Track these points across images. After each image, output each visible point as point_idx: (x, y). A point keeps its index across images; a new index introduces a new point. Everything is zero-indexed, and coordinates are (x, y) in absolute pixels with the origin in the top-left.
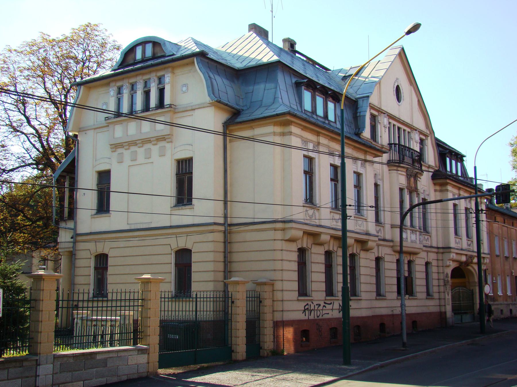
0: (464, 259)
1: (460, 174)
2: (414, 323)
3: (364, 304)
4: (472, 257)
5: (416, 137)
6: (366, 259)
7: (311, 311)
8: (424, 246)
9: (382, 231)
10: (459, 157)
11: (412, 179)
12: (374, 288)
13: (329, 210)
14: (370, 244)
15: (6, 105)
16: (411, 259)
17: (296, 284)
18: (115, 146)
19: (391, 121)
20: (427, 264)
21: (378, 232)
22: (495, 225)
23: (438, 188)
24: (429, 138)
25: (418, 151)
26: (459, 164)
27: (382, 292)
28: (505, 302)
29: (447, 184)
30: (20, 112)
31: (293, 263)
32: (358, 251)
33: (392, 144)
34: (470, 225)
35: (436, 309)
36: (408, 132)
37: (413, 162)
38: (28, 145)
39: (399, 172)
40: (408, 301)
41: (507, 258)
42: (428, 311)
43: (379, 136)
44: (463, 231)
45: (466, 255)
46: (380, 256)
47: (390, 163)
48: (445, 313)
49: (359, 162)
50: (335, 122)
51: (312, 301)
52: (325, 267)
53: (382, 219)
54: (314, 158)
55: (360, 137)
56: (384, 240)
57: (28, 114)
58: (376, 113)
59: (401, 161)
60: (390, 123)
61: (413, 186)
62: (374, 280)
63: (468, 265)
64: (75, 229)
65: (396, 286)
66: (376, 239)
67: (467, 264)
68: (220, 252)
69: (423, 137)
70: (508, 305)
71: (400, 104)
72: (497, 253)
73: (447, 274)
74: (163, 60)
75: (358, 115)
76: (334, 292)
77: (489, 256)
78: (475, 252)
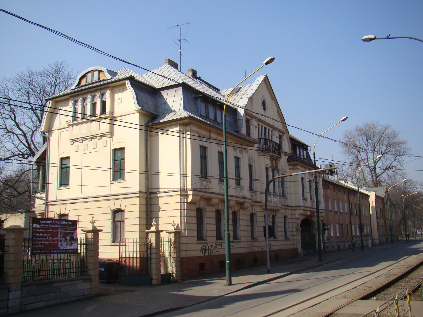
0: (309, 213)
1: (305, 157)
2: (277, 256)
3: (242, 245)
4: (314, 212)
5: (276, 133)
6: (244, 214)
7: (206, 250)
8: (283, 205)
10: (305, 147)
11: (274, 161)
14: (246, 205)
15: (4, 115)
17: (196, 232)
18: (74, 141)
19: (259, 123)
20: (285, 217)
21: (252, 197)
22: (329, 192)
23: (291, 167)
24: (285, 135)
25: (278, 143)
26: (305, 152)
27: (255, 236)
28: (335, 241)
29: (296, 165)
30: (12, 119)
31: (193, 218)
32: (238, 209)
33: (260, 138)
34: (312, 191)
35: (291, 247)
36: (271, 131)
37: (275, 150)
38: (17, 142)
39: (266, 157)
41: (336, 212)
42: (286, 248)
44: (308, 196)
45: (310, 211)
46: (253, 212)
47: (259, 150)
48: (297, 249)
49: (238, 150)
53: (254, 187)
55: (220, 93)
56: (256, 202)
57: (17, 121)
58: (249, 118)
60: (259, 125)
62: (249, 228)
63: (311, 218)
65: (263, 232)
66: (250, 201)
67: (311, 216)
69: (282, 134)
70: (337, 242)
72: (330, 209)
73: (298, 223)
74: (105, 82)
75: (238, 119)
76: (222, 237)
77: (325, 211)
78: (315, 208)
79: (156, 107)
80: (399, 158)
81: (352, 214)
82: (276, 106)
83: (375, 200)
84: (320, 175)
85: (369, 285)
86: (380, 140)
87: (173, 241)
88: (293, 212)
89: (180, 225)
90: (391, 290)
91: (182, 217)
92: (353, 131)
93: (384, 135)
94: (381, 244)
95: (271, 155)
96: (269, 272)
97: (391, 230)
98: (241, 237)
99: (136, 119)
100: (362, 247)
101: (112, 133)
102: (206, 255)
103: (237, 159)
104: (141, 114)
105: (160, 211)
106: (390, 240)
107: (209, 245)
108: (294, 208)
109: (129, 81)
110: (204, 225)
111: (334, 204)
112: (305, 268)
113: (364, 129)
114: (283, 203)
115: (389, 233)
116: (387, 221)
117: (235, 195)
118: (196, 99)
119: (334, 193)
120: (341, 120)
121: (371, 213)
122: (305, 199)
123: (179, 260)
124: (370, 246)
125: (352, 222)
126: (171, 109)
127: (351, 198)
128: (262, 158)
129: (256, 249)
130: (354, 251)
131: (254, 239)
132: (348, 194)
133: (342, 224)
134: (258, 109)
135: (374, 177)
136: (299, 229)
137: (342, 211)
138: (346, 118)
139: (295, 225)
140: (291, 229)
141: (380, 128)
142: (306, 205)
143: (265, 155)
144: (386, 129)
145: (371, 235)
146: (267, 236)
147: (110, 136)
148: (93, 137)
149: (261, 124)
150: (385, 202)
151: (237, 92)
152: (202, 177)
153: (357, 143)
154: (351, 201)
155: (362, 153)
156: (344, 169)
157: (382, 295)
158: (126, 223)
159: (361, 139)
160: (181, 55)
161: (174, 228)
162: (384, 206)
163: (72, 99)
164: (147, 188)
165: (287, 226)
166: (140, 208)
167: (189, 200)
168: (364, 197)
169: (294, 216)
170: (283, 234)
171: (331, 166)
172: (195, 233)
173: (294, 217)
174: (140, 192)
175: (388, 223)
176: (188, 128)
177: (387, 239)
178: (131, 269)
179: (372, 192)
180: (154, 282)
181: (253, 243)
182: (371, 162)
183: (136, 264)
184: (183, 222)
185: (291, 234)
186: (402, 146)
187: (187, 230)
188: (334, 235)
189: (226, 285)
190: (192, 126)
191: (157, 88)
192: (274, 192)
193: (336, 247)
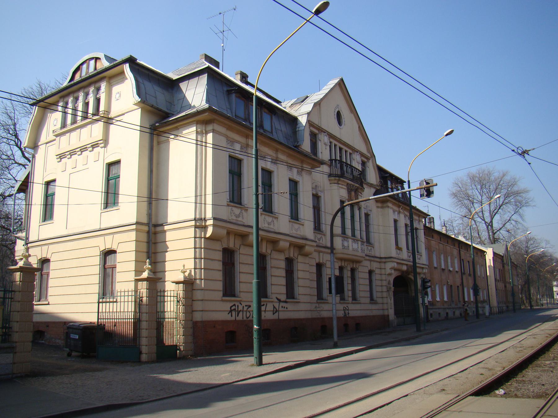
0: (404, 268)
3: (302, 307)
7: (239, 312)
8: (366, 255)
9: (324, 239)
14: (307, 249)
16: (355, 266)
18: (61, 157)
19: (331, 140)
20: (370, 272)
22: (433, 243)
23: (379, 205)
24: (371, 161)
28: (442, 307)
32: (296, 255)
36: (350, 154)
39: (340, 186)
40: (352, 305)
41: (443, 270)
42: (371, 314)
43: (320, 152)
45: (407, 265)
46: (321, 261)
48: (388, 316)
49: (295, 170)
50: (272, 132)
51: (240, 302)
58: (316, 131)
59: (342, 175)
60: (331, 142)
64: (27, 238)
67: (407, 272)
68: (144, 252)
75: (297, 129)
79: (171, 104)
80: (520, 211)
81: (464, 274)
83: (493, 258)
84: (421, 219)
85: (489, 366)
86: (497, 188)
87: (181, 295)
88: (383, 265)
89: (193, 271)
90: (530, 373)
92: (465, 178)
93: (502, 182)
94: (501, 312)
95: (348, 184)
96: (335, 346)
97: (513, 295)
98: (300, 296)
99: (136, 117)
100: (477, 315)
101: (106, 141)
102: (238, 319)
103: (294, 184)
104: (144, 111)
105: (167, 251)
106: (511, 308)
108: (383, 260)
109: (128, 65)
110: (237, 275)
111: (440, 259)
112: (392, 340)
113: (478, 175)
114: (367, 252)
115: (510, 299)
116: (507, 285)
117: (288, 233)
118: (229, 92)
119: (441, 245)
120: (445, 134)
121: (488, 274)
122: (398, 248)
124: (487, 314)
125: (465, 284)
126: (190, 105)
127: (462, 253)
128: (335, 186)
129: (325, 314)
130: (466, 320)
131: (322, 299)
132: (459, 247)
133: (451, 286)
135: (491, 234)
136: (390, 288)
137: (451, 269)
138: (452, 132)
139: (385, 283)
140: (379, 289)
141: (496, 174)
142: (401, 257)
144: (504, 175)
145: (488, 301)
146: (333, 291)
147: (103, 145)
148: (83, 149)
149: (334, 142)
150: (505, 261)
151: (302, 102)
152: (232, 201)
153: (470, 192)
154: (463, 257)
155: (476, 205)
156: (454, 225)
157: (515, 384)
158: (118, 269)
159: (473, 186)
160: (224, 50)
161: (185, 277)
162: (503, 267)
163: (62, 100)
164: (150, 215)
165: (374, 284)
166: (137, 246)
167: (209, 234)
168: (479, 253)
170: (368, 294)
171: (427, 183)
172: (219, 286)
174: (137, 223)
175: (509, 287)
176: (210, 127)
177: (507, 307)
178: (122, 337)
179: (489, 249)
180: (144, 357)
181: (321, 305)
182: (487, 215)
183: (129, 331)
184: (198, 267)
185: (379, 295)
186: (524, 195)
187: (204, 279)
189: (253, 365)
190: (215, 125)
191: (174, 79)
192: (353, 235)
193: (443, 315)
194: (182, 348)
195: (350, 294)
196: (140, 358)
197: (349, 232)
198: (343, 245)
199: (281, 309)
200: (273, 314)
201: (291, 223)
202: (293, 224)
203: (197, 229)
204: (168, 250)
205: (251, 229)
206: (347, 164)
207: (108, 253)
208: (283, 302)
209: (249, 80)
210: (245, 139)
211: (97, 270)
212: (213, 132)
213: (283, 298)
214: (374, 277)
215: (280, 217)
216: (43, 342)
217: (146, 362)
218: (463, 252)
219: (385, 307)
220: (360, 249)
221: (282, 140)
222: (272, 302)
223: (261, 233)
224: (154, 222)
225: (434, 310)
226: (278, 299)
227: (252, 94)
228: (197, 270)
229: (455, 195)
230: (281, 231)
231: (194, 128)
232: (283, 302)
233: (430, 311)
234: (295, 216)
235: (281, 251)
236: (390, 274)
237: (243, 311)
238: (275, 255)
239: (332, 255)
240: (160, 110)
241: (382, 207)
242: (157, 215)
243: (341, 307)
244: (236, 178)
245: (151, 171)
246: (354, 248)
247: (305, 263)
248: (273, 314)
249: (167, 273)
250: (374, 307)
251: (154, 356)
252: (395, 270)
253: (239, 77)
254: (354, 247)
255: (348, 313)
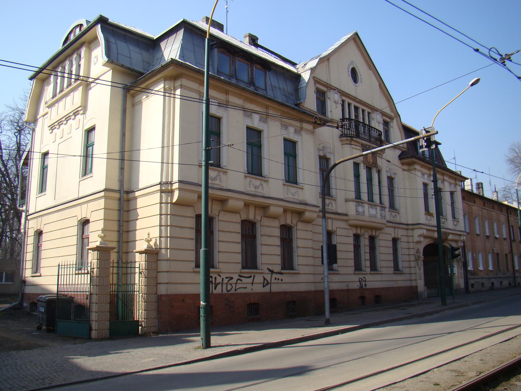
3: (302, 278)
8: (388, 222)
9: (398, 217)
12: (391, 264)
13: (281, 183)
14: (308, 215)
16: (374, 234)
18: (52, 128)
19: (344, 98)
20: (395, 241)
23: (406, 167)
24: (395, 121)
28: (487, 276)
32: (295, 222)
36: (369, 113)
39: (353, 146)
41: (488, 237)
42: (395, 285)
46: (397, 237)
48: (416, 287)
49: (256, 117)
50: (266, 90)
52: (281, 241)
54: (263, 131)
58: (324, 89)
59: (358, 136)
61: (371, 161)
71: (356, 85)
73: (418, 250)
75: (299, 87)
81: (514, 241)
82: (377, 79)
88: (410, 233)
89: (158, 239)
91: (163, 228)
96: (328, 323)
101: (84, 107)
104: (115, 72)
107: (223, 276)
108: (411, 227)
111: (493, 226)
114: (388, 218)
119: (484, 210)
123: (154, 298)
132: (507, 213)
134: (341, 80)
137: (497, 236)
139: (412, 252)
140: (406, 258)
142: (458, 228)
143: (352, 143)
147: (81, 112)
148: (67, 118)
149: (347, 100)
154: (512, 223)
160: (227, 12)
164: (121, 182)
169: (411, 239)
171: (427, 132)
173: (411, 239)
174: (105, 190)
176: (178, 83)
180: (94, 334)
184: (163, 235)
185: (406, 264)
188: (483, 267)
189: (199, 348)
190: (183, 79)
193: (487, 284)
194: (143, 323)
195: (368, 263)
196: (90, 334)
197: (365, 197)
198: (357, 211)
199: (273, 281)
200: (264, 287)
201: (286, 187)
202: (289, 188)
203: (163, 194)
204: (139, 218)
205: (199, 187)
206: (364, 124)
207: (85, 223)
208: (277, 273)
209: (259, 42)
210: (225, 95)
211: (74, 240)
212: (181, 88)
213: (278, 268)
214: (400, 245)
215: (306, 187)
216: (36, 313)
217: (95, 339)
218: (512, 219)
219: (413, 277)
220: (379, 216)
221: (280, 98)
222: (263, 273)
223: (210, 191)
224: (126, 188)
225: (476, 280)
226: (269, 270)
227: (205, 32)
228: (162, 239)
229: (511, 161)
230: (272, 195)
231: (162, 85)
232: (277, 273)
233: (471, 282)
234: (291, 178)
235: (274, 217)
236: (419, 242)
237: (222, 283)
238: (266, 222)
239: (324, 219)
240: (133, 70)
241: (409, 170)
242: (130, 181)
243: (356, 278)
244: (291, 158)
245: (123, 135)
246: (370, 214)
247: (307, 231)
248: (264, 287)
249: (137, 243)
250: (399, 277)
251: (107, 333)
252: (425, 237)
253: (247, 39)
254: (371, 213)
255: (365, 285)
